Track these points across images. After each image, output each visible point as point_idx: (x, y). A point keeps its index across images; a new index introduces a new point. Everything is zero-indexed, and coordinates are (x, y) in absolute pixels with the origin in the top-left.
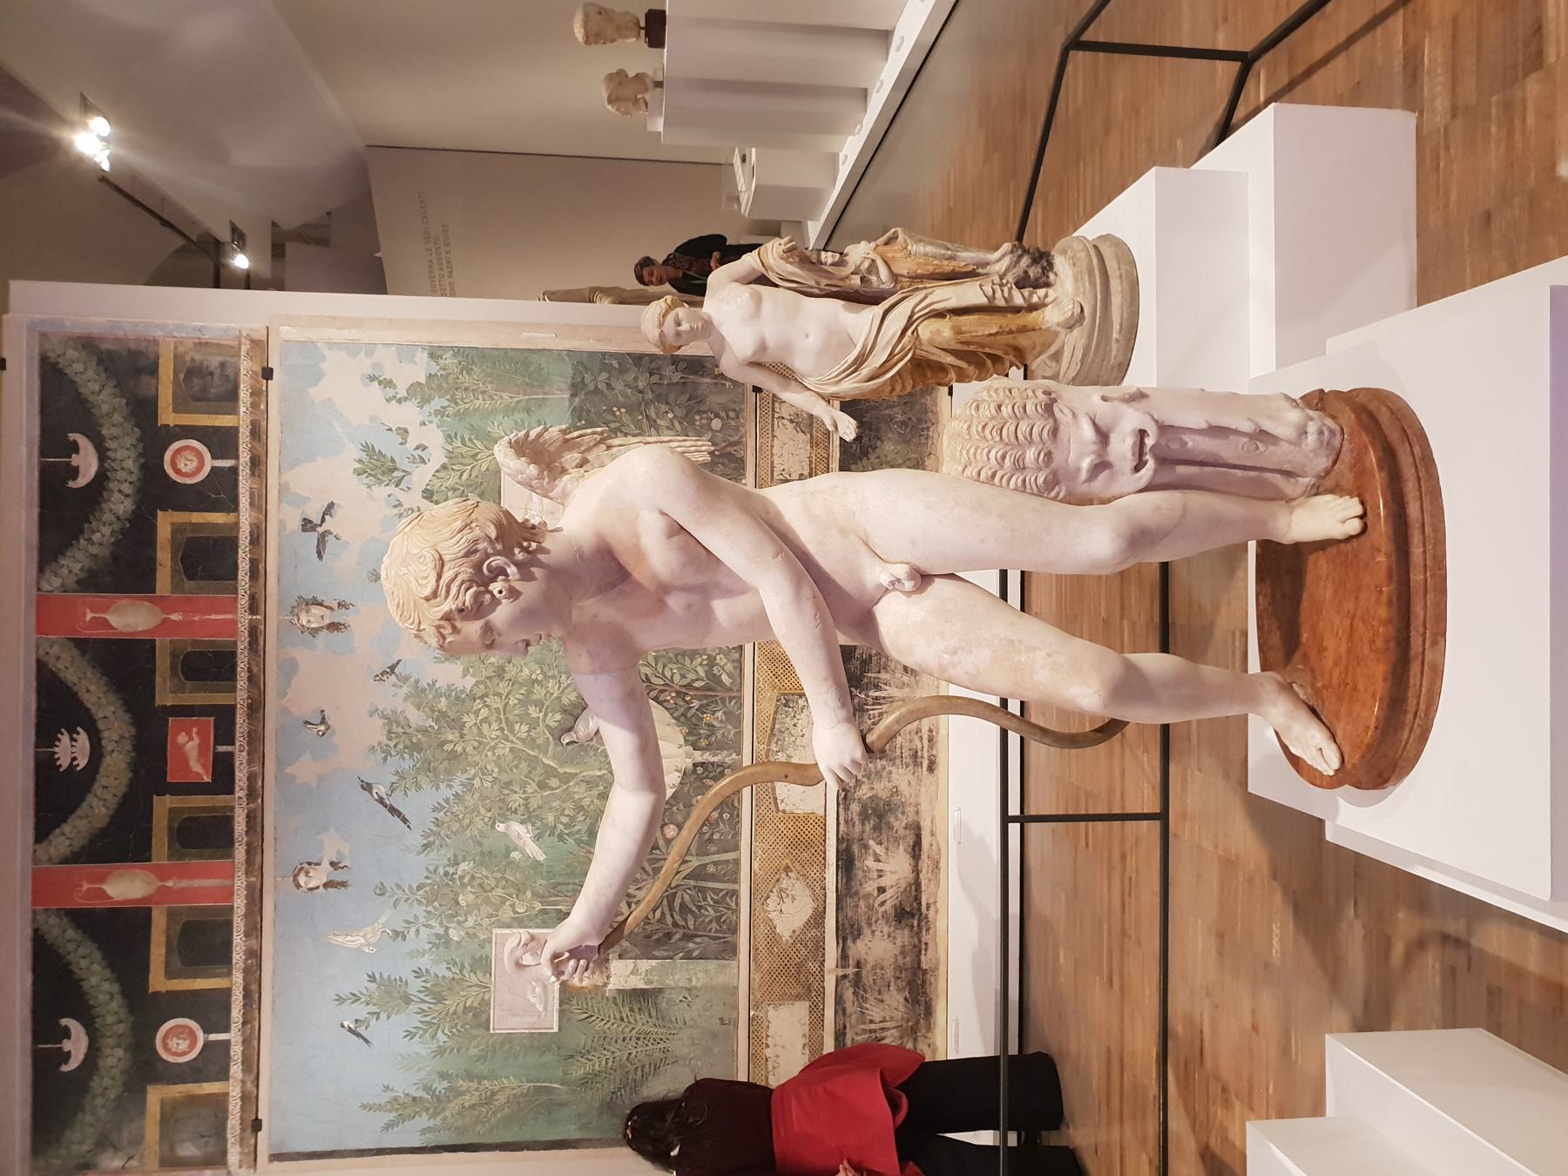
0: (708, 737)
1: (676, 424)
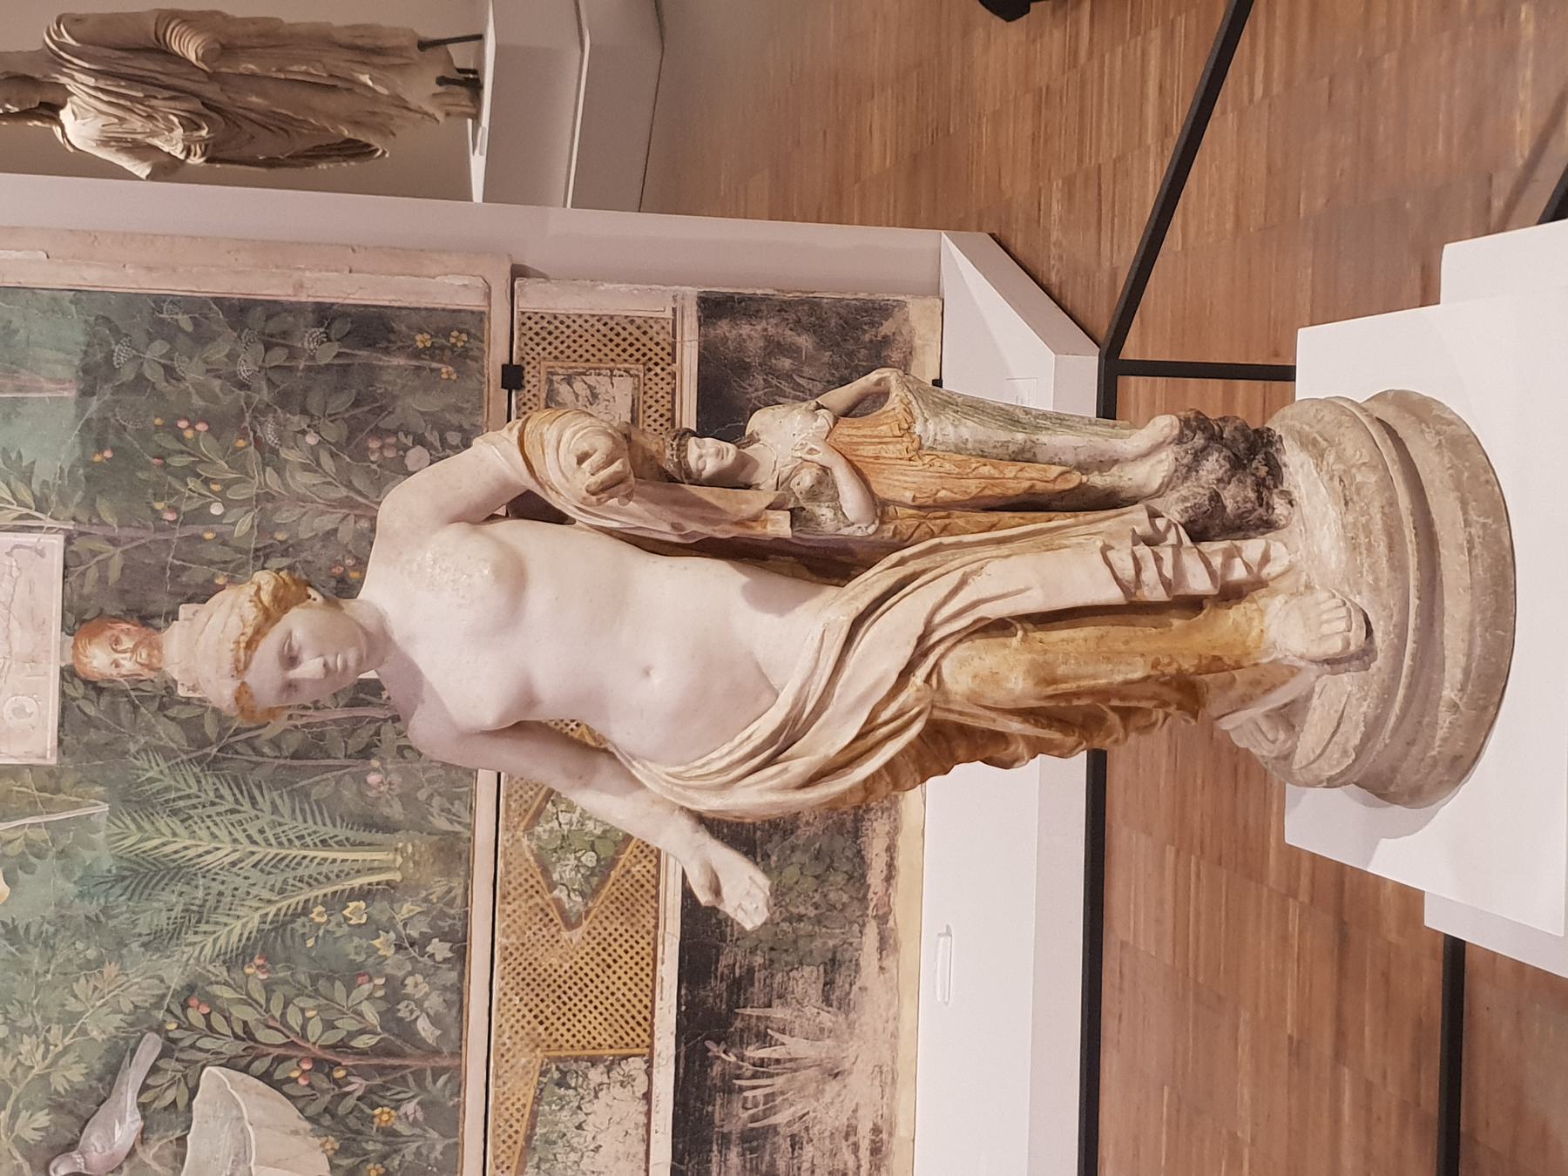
0: (383, 1158)
1: (325, 459)
